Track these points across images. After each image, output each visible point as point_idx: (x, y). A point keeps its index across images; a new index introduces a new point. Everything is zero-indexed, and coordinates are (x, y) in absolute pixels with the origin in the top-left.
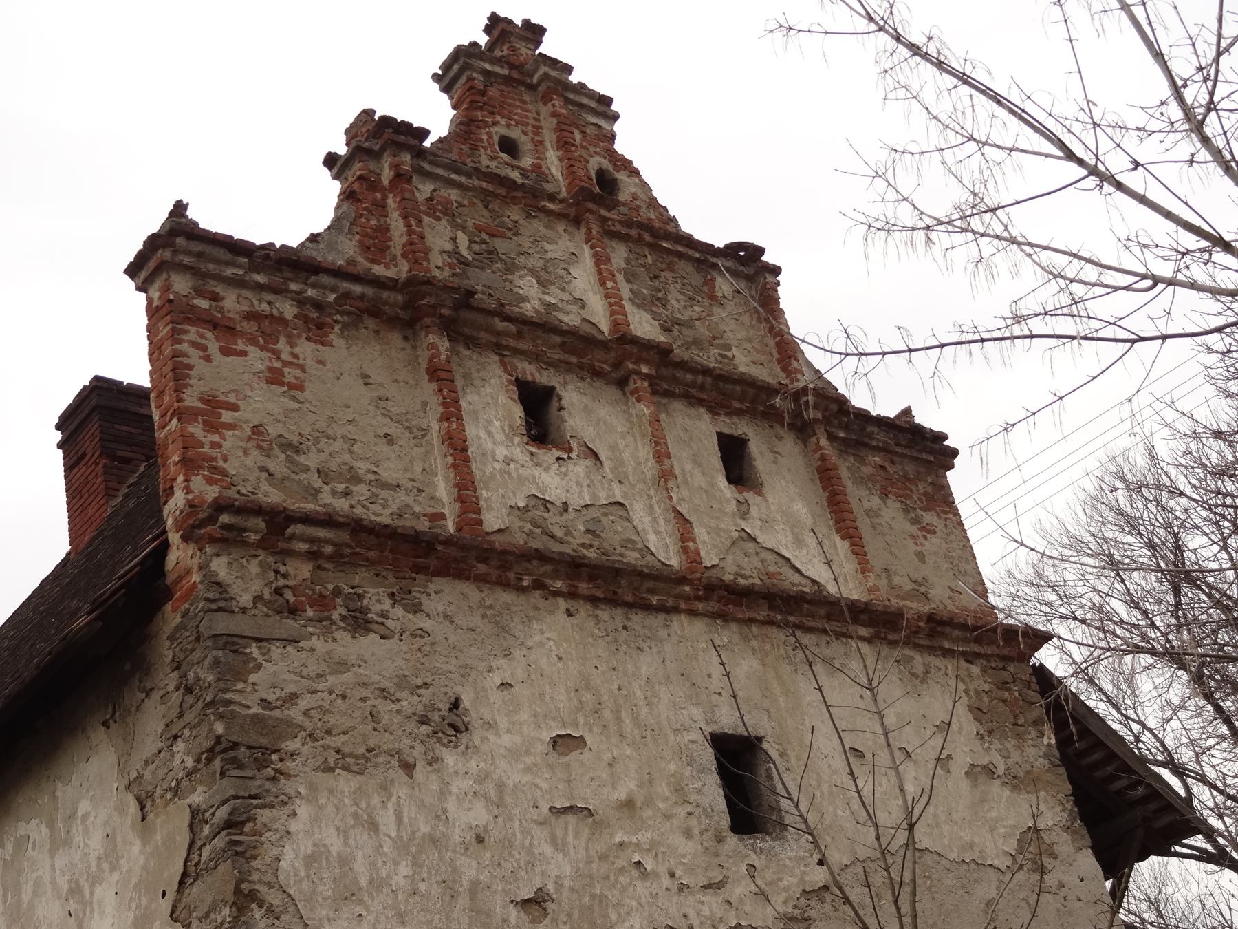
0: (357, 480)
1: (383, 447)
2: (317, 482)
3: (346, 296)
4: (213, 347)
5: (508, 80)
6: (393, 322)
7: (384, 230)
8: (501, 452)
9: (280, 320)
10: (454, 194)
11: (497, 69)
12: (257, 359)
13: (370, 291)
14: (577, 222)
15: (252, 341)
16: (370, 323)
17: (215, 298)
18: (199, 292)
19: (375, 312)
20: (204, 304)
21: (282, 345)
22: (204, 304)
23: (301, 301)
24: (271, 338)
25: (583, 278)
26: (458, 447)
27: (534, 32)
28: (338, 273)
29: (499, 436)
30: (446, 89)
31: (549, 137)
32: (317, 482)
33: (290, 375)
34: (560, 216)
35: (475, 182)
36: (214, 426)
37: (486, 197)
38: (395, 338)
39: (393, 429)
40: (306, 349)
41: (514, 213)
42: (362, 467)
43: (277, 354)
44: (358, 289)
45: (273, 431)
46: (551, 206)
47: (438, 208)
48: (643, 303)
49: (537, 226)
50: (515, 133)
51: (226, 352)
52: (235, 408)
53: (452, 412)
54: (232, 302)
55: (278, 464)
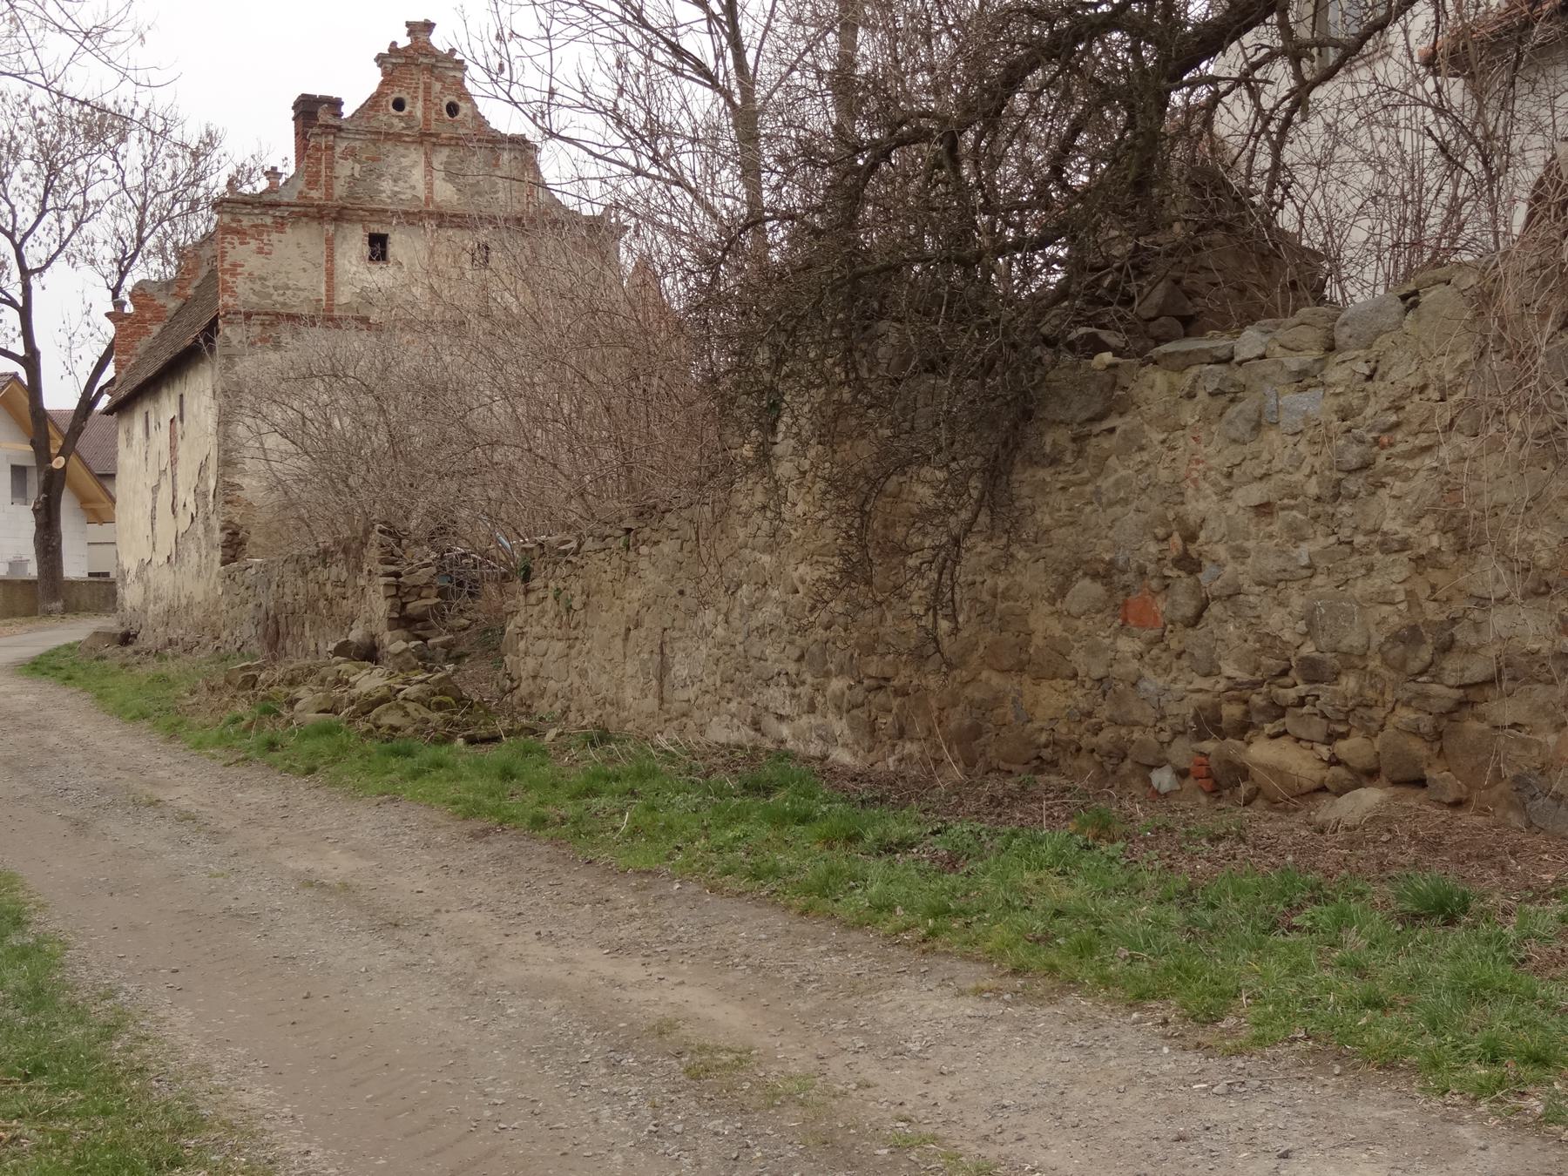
0: (289, 288)
1: (302, 274)
2: (271, 290)
3: (293, 212)
4: (236, 242)
5: (405, 64)
6: (313, 218)
7: (318, 172)
8: (354, 269)
9: (266, 226)
10: (358, 144)
11: (399, 61)
12: (253, 244)
13: (302, 209)
14: (421, 143)
15: (253, 237)
16: (305, 219)
17: (240, 221)
18: (233, 220)
19: (306, 215)
20: (234, 225)
21: (265, 237)
22: (234, 225)
23: (274, 217)
24: (261, 234)
25: (417, 175)
26: (330, 274)
27: (428, 26)
28: (289, 205)
29: (354, 262)
30: (380, 66)
31: (421, 93)
32: (271, 290)
33: (266, 249)
34: (413, 142)
35: (369, 136)
36: (234, 275)
37: (374, 142)
38: (315, 224)
39: (307, 265)
40: (275, 236)
41: (388, 146)
42: (291, 283)
43: (262, 240)
44: (297, 209)
45: (256, 274)
46: (407, 139)
47: (351, 153)
48: (451, 176)
49: (401, 150)
50: (403, 95)
51: (241, 244)
52: (242, 266)
53: (331, 258)
54: (246, 222)
55: (257, 287)
